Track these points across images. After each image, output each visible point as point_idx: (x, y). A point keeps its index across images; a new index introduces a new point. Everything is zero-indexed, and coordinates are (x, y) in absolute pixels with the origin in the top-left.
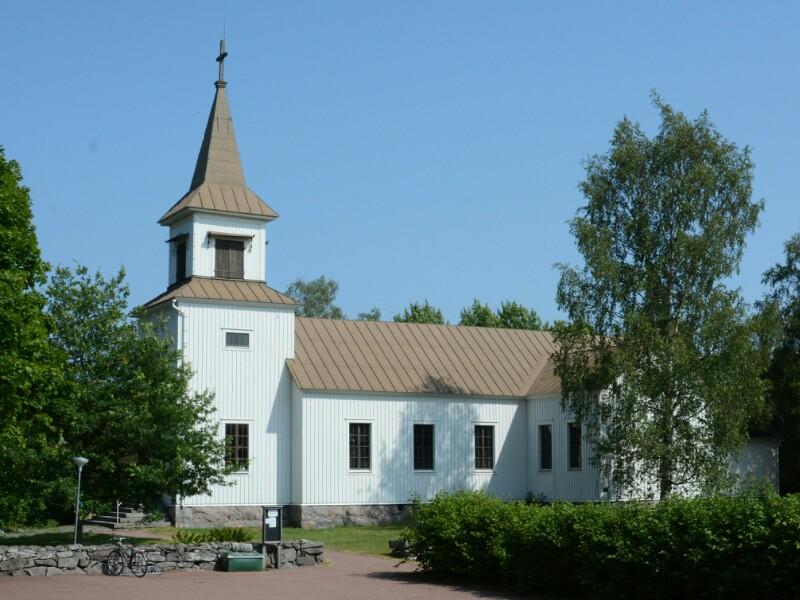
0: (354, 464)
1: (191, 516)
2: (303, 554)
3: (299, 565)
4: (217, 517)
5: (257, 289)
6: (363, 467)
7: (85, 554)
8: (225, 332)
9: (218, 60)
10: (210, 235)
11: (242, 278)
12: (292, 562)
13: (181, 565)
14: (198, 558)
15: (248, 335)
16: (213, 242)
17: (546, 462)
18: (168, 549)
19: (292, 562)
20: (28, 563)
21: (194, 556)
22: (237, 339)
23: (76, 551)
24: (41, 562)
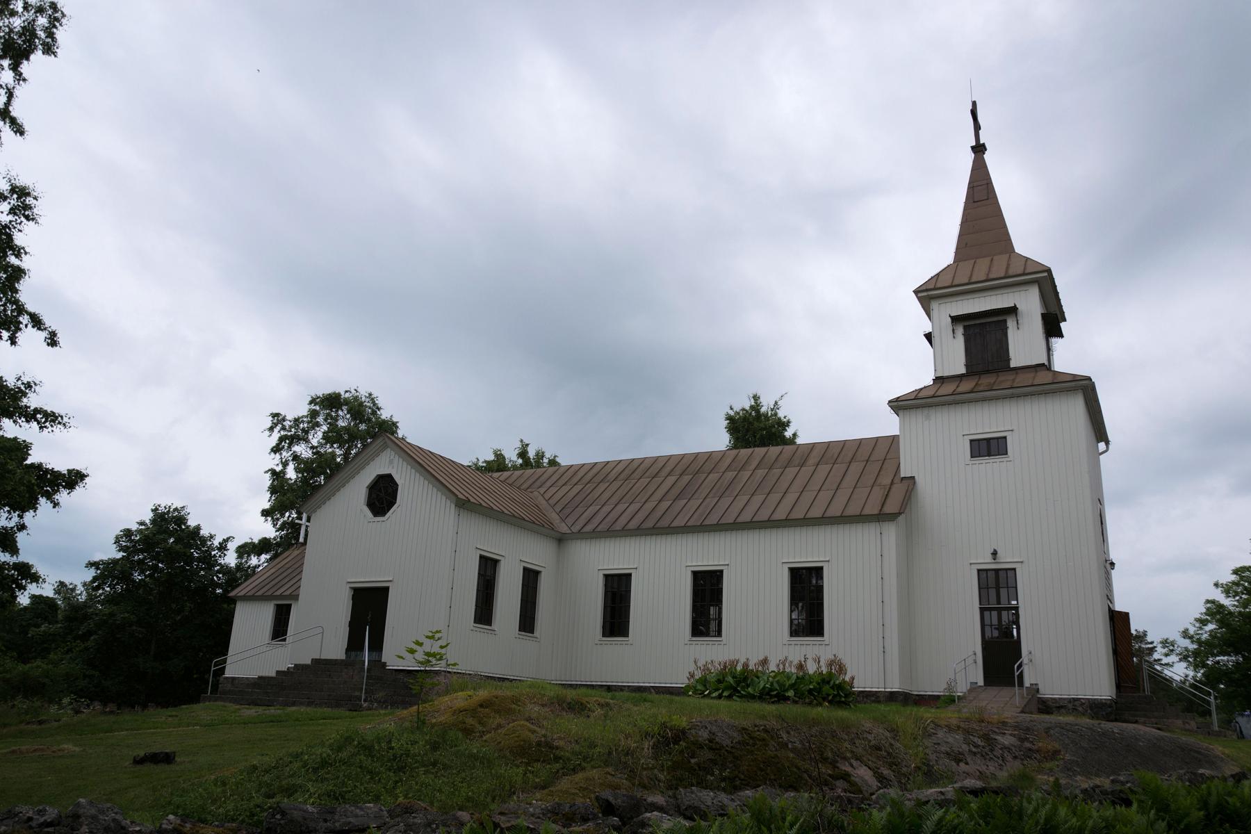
10: (956, 320)
16: (960, 331)
22: (989, 447)
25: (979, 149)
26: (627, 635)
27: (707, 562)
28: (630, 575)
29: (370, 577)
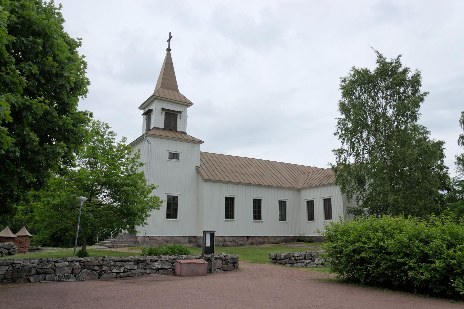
1: (148, 241)
2: (226, 263)
3: (224, 270)
4: (162, 242)
5: (13, 136)
6: (173, 218)
7: (78, 264)
9: (168, 41)
10: (163, 109)
11: (176, 129)
12: (219, 268)
13: (148, 271)
14: (160, 266)
16: (164, 113)
17: (311, 217)
18: (140, 260)
19: (219, 268)
20: (30, 271)
21: (157, 265)
22: (174, 156)
23: (71, 262)
24: (41, 271)
25: (169, 50)
26: (314, 220)
27: (327, 196)
28: (330, 199)
29: (173, 193)
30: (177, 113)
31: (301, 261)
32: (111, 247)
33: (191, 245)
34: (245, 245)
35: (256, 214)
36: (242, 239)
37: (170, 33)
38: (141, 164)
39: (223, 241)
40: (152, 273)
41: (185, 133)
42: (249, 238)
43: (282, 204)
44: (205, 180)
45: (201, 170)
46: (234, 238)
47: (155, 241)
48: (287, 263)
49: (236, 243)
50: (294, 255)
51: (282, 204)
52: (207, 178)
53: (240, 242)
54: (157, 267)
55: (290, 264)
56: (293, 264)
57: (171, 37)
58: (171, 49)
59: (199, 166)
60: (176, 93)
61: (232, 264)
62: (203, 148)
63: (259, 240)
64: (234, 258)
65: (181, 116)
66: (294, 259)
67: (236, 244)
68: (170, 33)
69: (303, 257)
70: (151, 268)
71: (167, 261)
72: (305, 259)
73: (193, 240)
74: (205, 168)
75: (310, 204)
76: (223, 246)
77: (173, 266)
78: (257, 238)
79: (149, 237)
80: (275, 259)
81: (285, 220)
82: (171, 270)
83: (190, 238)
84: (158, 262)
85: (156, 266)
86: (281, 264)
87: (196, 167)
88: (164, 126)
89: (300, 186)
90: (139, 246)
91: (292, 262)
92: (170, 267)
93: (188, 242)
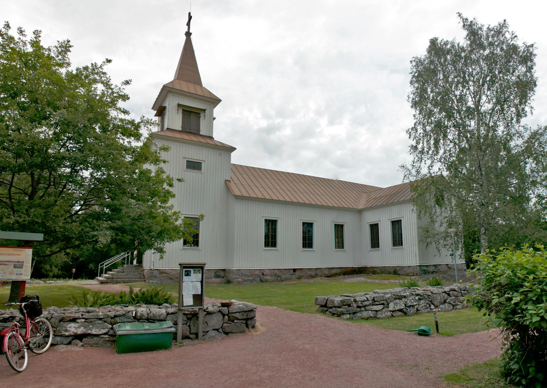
0: (267, 244)
1: (158, 275)
3: (227, 333)
8: (186, 160)
10: (179, 105)
11: (199, 133)
12: (217, 330)
15: (201, 163)
16: (181, 111)
19: (217, 330)
22: (194, 166)
25: (188, 34)
30: (199, 112)
31: (367, 308)
32: (104, 283)
33: (218, 280)
34: (291, 279)
35: (306, 240)
36: (287, 272)
37: (190, 14)
38: (485, 315)
39: (261, 275)
40: (62, 344)
41: (211, 138)
42: (297, 270)
43: (339, 229)
44: (237, 197)
45: (232, 185)
46: (276, 271)
47: (167, 275)
48: (345, 312)
49: (278, 277)
50: (355, 300)
51: (339, 229)
52: (239, 194)
53: (283, 277)
54: (74, 332)
55: (349, 314)
56: (354, 313)
57: (190, 18)
58: (191, 34)
59: (230, 179)
60: (198, 87)
61: (242, 321)
62: (236, 158)
63: (309, 272)
64: (246, 311)
65: (205, 116)
66: (355, 306)
67: (279, 278)
68: (190, 14)
69: (371, 302)
70: (60, 334)
71: (100, 319)
72: (373, 305)
73: (222, 274)
74: (237, 182)
75: (374, 228)
76: (261, 280)
77: (112, 328)
78: (306, 270)
79: (158, 269)
80: (325, 306)
81: (343, 247)
82: (107, 336)
83: (217, 271)
84: (78, 322)
85: (71, 329)
86: (335, 314)
87: (226, 180)
88: (182, 127)
89: (361, 207)
90: (145, 281)
91: (352, 311)
92: (105, 331)
93: (215, 276)
